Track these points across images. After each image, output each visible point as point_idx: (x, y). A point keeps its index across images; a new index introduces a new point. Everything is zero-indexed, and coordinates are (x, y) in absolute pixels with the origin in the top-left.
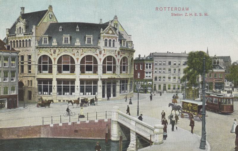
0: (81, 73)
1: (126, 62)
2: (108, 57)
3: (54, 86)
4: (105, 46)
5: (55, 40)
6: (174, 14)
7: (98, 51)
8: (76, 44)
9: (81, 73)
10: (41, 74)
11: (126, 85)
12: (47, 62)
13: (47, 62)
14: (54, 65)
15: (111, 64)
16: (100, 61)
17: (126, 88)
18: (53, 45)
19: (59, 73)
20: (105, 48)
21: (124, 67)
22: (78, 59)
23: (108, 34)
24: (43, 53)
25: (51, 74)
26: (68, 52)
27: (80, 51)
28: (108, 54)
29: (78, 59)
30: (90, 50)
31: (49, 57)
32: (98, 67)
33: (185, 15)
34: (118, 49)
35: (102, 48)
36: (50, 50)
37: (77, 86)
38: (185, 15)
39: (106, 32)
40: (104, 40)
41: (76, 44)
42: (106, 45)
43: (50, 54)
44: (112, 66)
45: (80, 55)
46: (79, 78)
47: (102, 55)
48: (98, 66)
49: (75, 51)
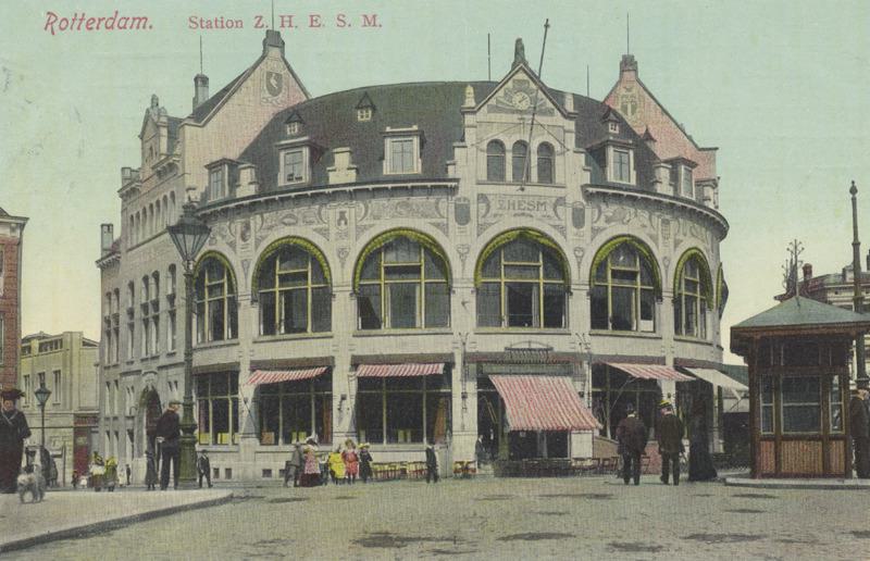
0: (363, 327)
3: (343, 398)
5: (342, 159)
6: (201, 21)
8: (333, 178)
9: (363, 327)
10: (222, 343)
11: (233, 399)
17: (317, 418)
18: (331, 182)
19: (365, 325)
20: (490, 190)
22: (342, 253)
26: (418, 216)
27: (354, 210)
28: (510, 222)
33: (256, 27)
34: (575, 196)
35: (467, 190)
37: (464, 397)
38: (256, 27)
41: (333, 178)
42: (495, 173)
45: (353, 233)
46: (350, 353)
47: (472, 226)
49: (331, 212)
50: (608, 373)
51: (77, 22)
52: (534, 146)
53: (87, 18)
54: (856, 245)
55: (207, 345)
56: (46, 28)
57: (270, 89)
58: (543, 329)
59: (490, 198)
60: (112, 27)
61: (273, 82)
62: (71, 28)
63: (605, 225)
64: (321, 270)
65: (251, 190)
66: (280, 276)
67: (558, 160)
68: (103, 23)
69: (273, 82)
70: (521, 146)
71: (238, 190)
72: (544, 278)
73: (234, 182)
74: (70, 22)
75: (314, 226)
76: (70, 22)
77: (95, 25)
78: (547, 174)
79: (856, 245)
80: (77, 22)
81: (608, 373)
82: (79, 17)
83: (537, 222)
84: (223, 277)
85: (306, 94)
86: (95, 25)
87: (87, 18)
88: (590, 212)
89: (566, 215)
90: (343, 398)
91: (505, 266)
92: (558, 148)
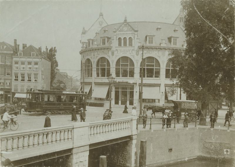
1: (90, 65)
2: (101, 58)
4: (119, 45)
7: (110, 53)
12: (154, 65)
13: (128, 64)
14: (136, 67)
15: (153, 66)
16: (113, 63)
21: (103, 70)
23: (122, 31)
24: (147, 54)
25: (133, 78)
29: (94, 62)
30: (103, 52)
31: (107, 60)
32: (111, 70)
36: (108, 51)
37: (136, 92)
39: (119, 29)
40: (117, 39)
42: (120, 44)
43: (91, 57)
44: (170, 69)
48: (111, 68)
52: (122, 39)
55: (87, 78)
58: (129, 78)
59: (118, 50)
61: (101, 23)
64: (132, 64)
66: (121, 64)
67: (133, 41)
69: (101, 23)
70: (125, 38)
72: (129, 66)
78: (131, 44)
83: (128, 55)
84: (105, 63)
85: (107, 24)
90: (136, 92)
91: (101, 65)
92: (133, 38)
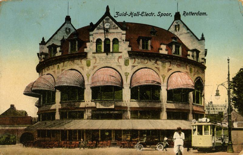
42: (98, 51)
50: (51, 92)
51: (190, 14)
53: (192, 13)
54: (229, 75)
56: (183, 15)
57: (66, 32)
60: (198, 15)
62: (189, 15)
63: (137, 65)
65: (60, 54)
68: (196, 14)
69: (68, 31)
71: (56, 54)
73: (55, 52)
74: (189, 14)
75: (79, 66)
76: (189, 14)
77: (194, 15)
79: (229, 75)
80: (190, 14)
81: (51, 92)
82: (191, 12)
86: (194, 15)
87: (200, 12)
88: (131, 62)
89: (122, 62)
